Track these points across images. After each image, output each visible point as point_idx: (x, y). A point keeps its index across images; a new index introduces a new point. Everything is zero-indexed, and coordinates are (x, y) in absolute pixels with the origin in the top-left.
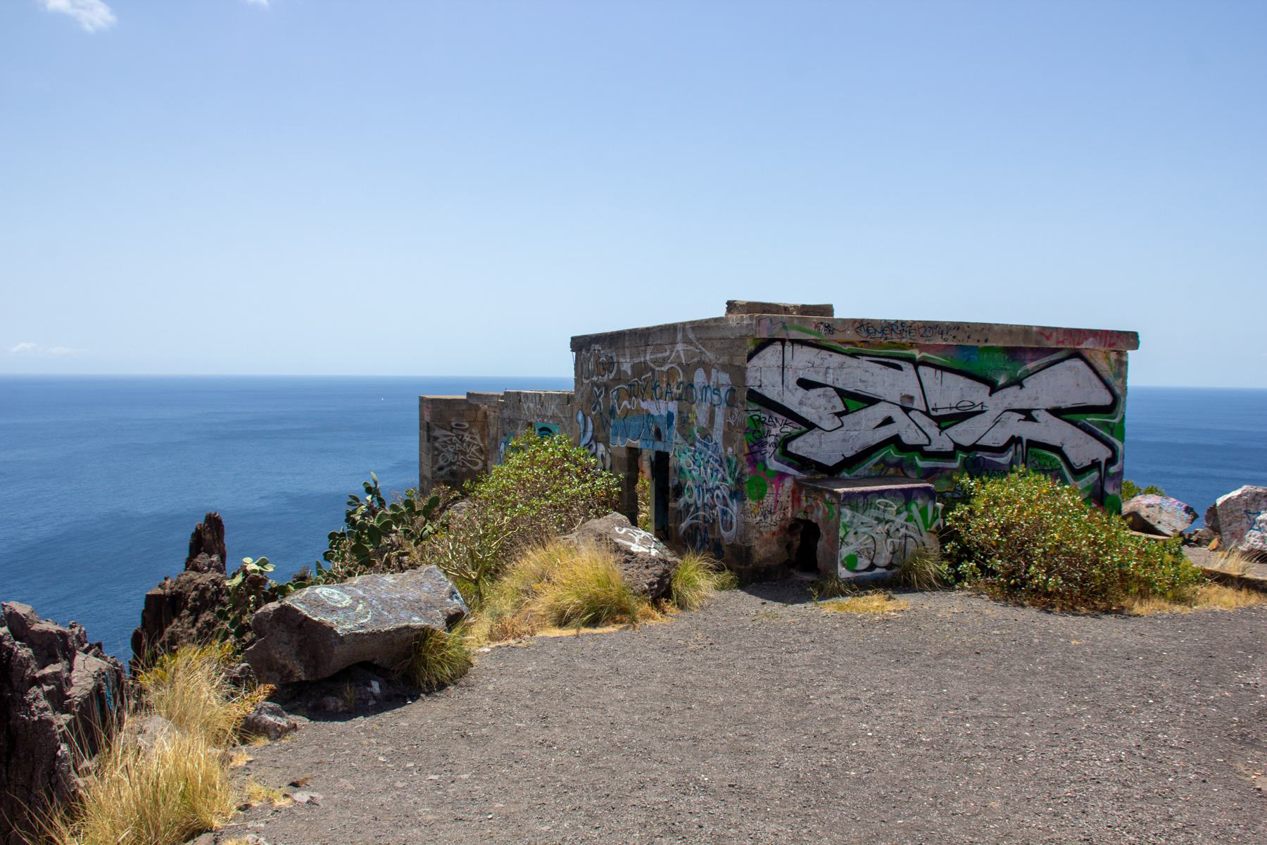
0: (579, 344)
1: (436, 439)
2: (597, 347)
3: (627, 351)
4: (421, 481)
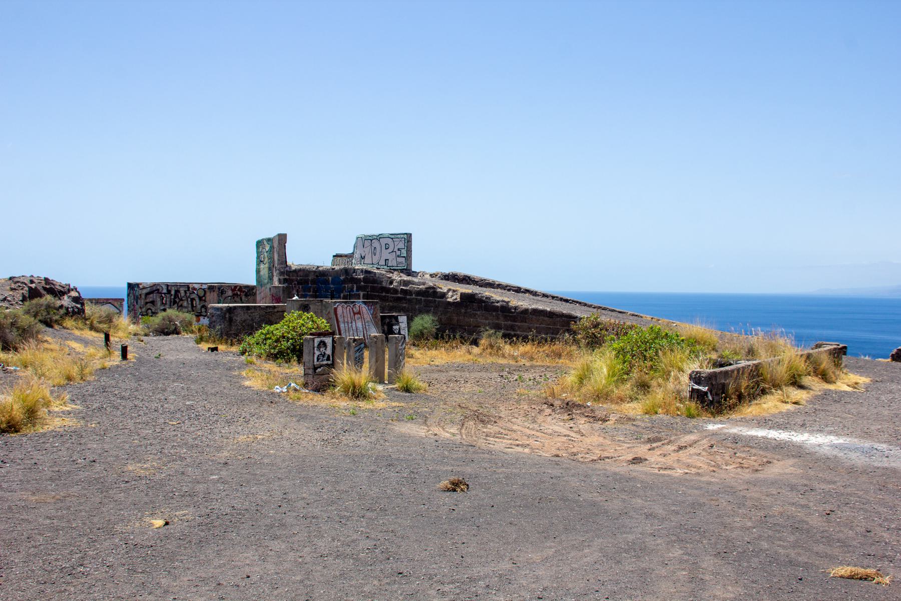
0: (131, 286)
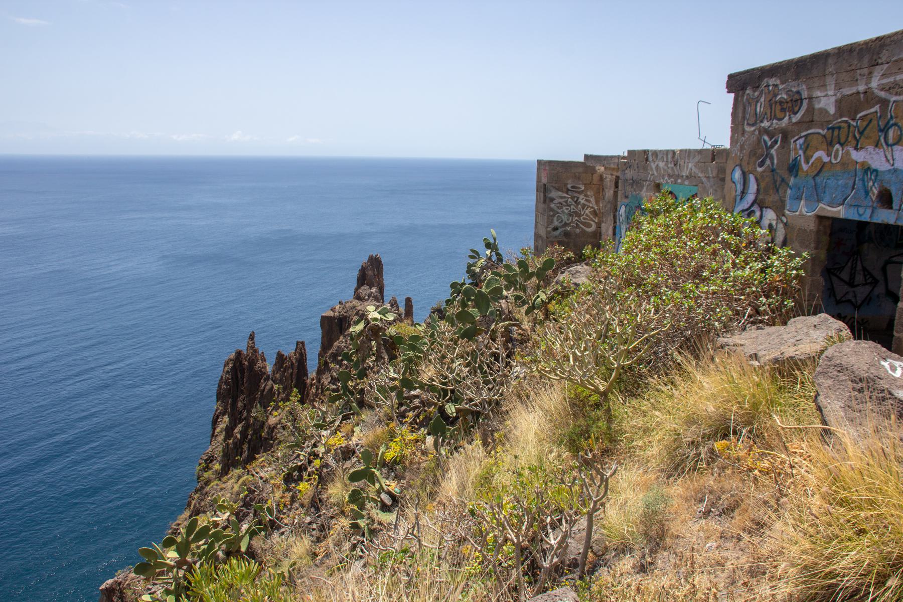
0: (740, 83)
1: (552, 200)
2: (772, 81)
3: (831, 81)
4: (536, 240)
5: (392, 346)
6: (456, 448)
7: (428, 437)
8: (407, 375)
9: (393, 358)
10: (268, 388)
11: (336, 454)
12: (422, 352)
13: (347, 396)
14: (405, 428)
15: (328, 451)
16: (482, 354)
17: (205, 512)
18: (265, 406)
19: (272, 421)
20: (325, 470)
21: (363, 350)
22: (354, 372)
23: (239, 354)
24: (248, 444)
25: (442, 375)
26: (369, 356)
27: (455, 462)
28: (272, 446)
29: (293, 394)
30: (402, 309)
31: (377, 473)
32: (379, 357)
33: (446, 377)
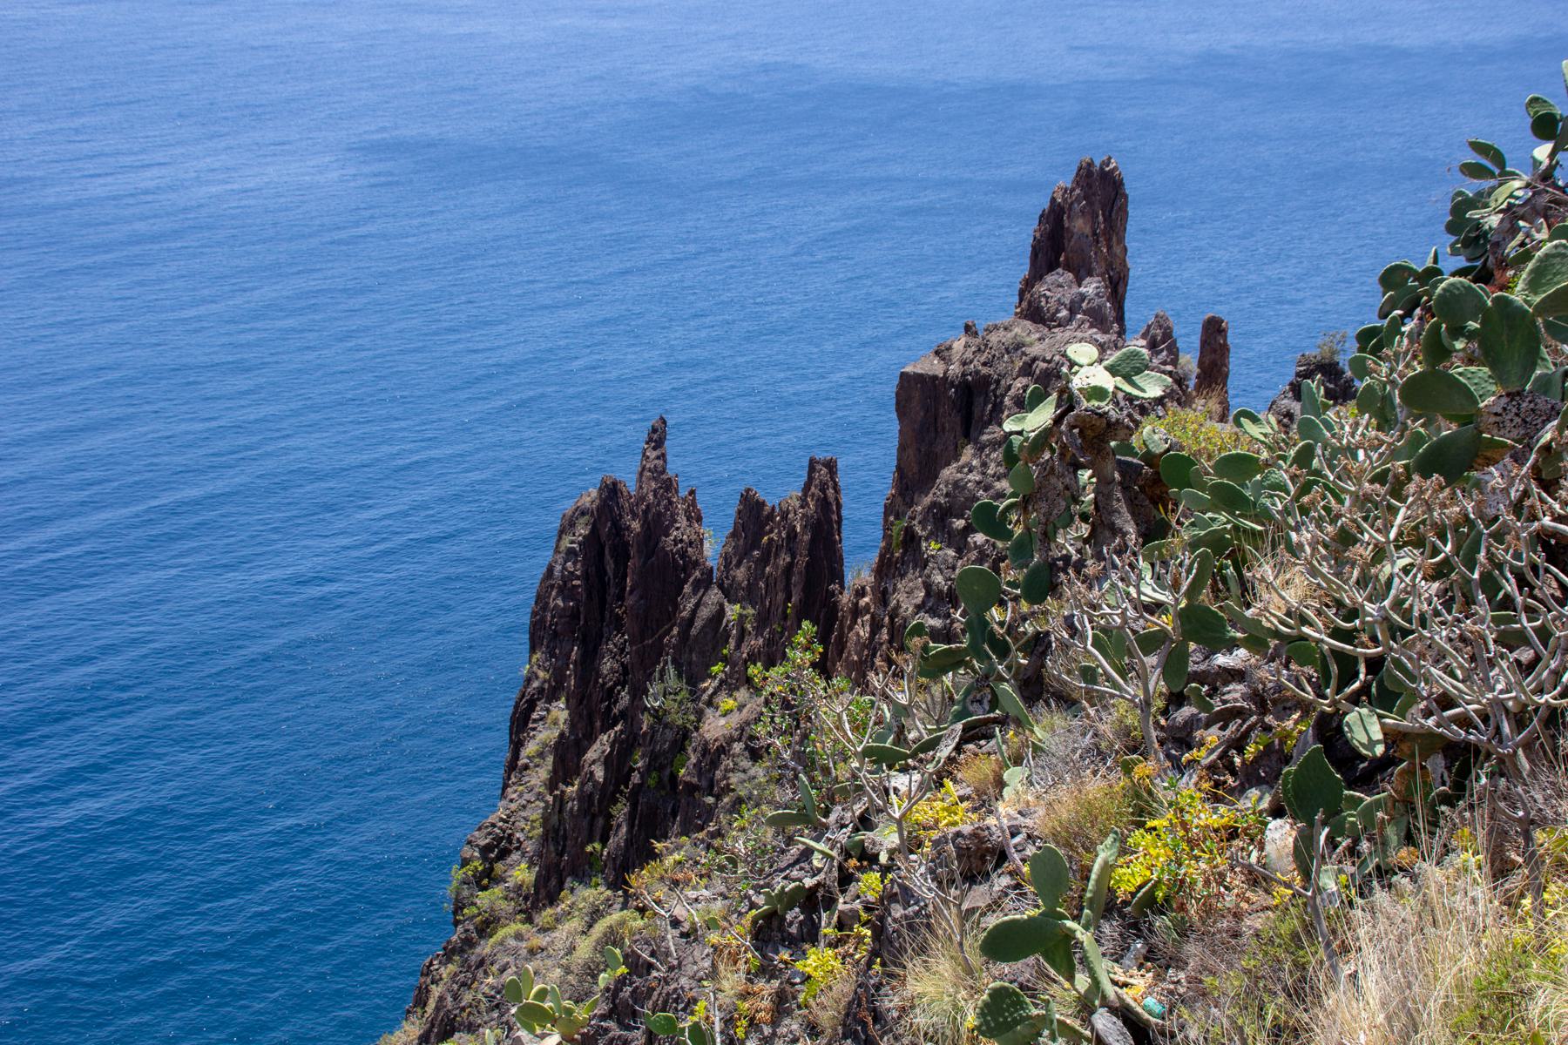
5: (1152, 489)
6: (1383, 873)
7: (1274, 824)
8: (1205, 596)
9: (1153, 531)
10: (705, 613)
11: (939, 859)
12: (1263, 516)
13: (983, 657)
14: (1189, 785)
15: (911, 844)
16: (1499, 537)
17: (471, 1028)
18: (693, 678)
19: (715, 727)
20: (898, 911)
21: (1045, 498)
22: (1012, 575)
23: (611, 491)
24: (631, 805)
25: (1339, 604)
26: (1069, 522)
27: (1378, 924)
28: (709, 813)
29: (800, 639)
30: (1189, 361)
31: (1084, 936)
32: (1102, 528)
33: (1352, 614)
